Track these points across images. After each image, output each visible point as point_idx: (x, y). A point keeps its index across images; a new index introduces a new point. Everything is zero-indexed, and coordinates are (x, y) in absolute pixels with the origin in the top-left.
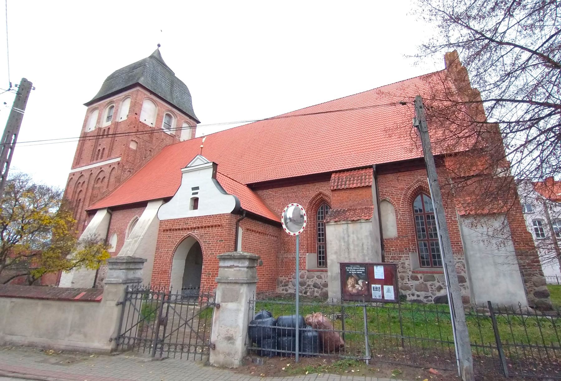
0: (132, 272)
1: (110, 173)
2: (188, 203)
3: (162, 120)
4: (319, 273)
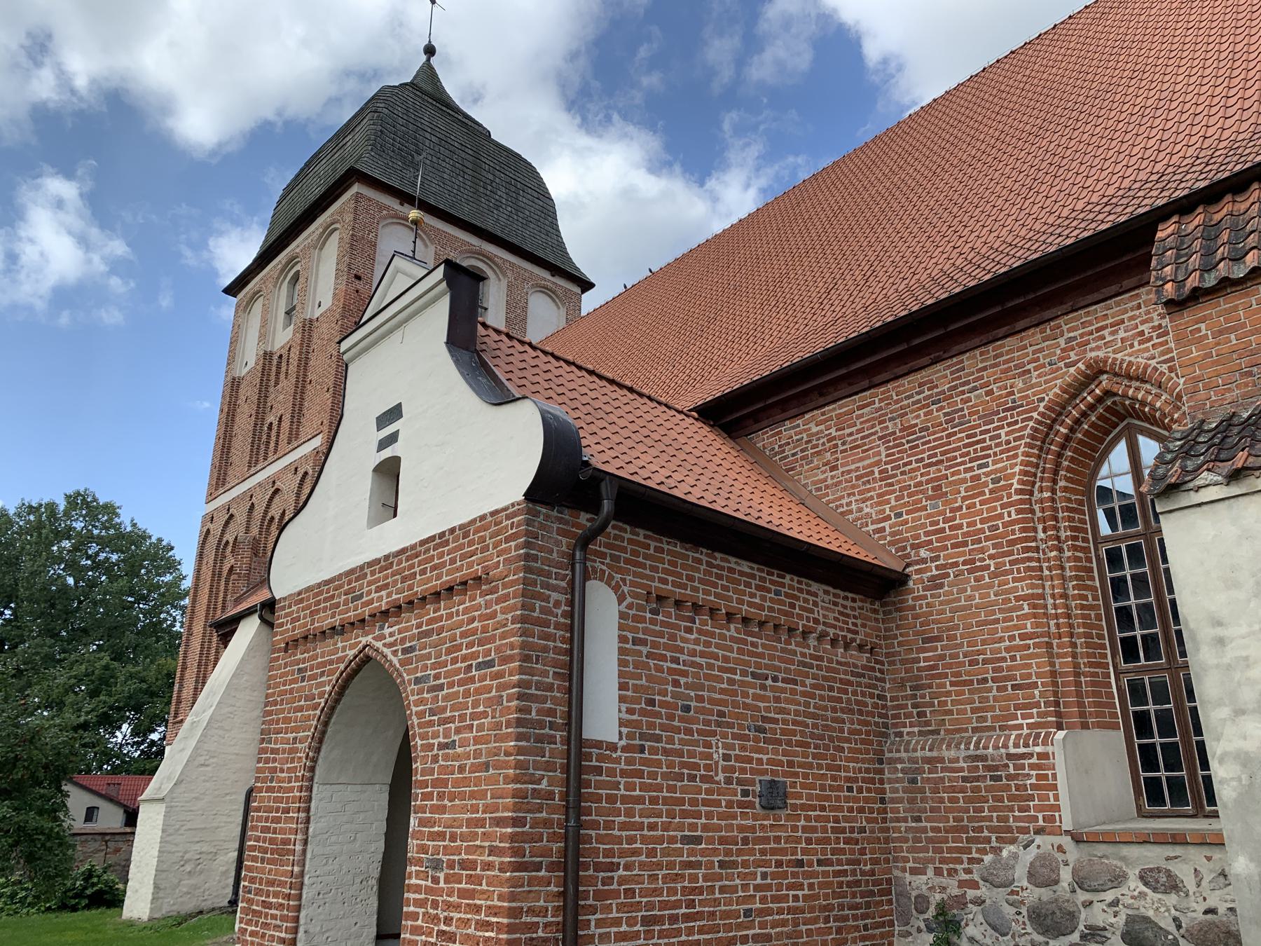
4: (1154, 856)
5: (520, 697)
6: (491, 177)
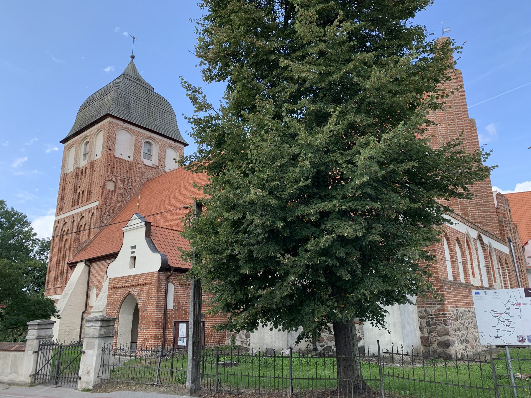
0: (43, 331)
1: (91, 220)
2: (128, 261)
3: (141, 150)
5: (157, 303)
6: (154, 109)
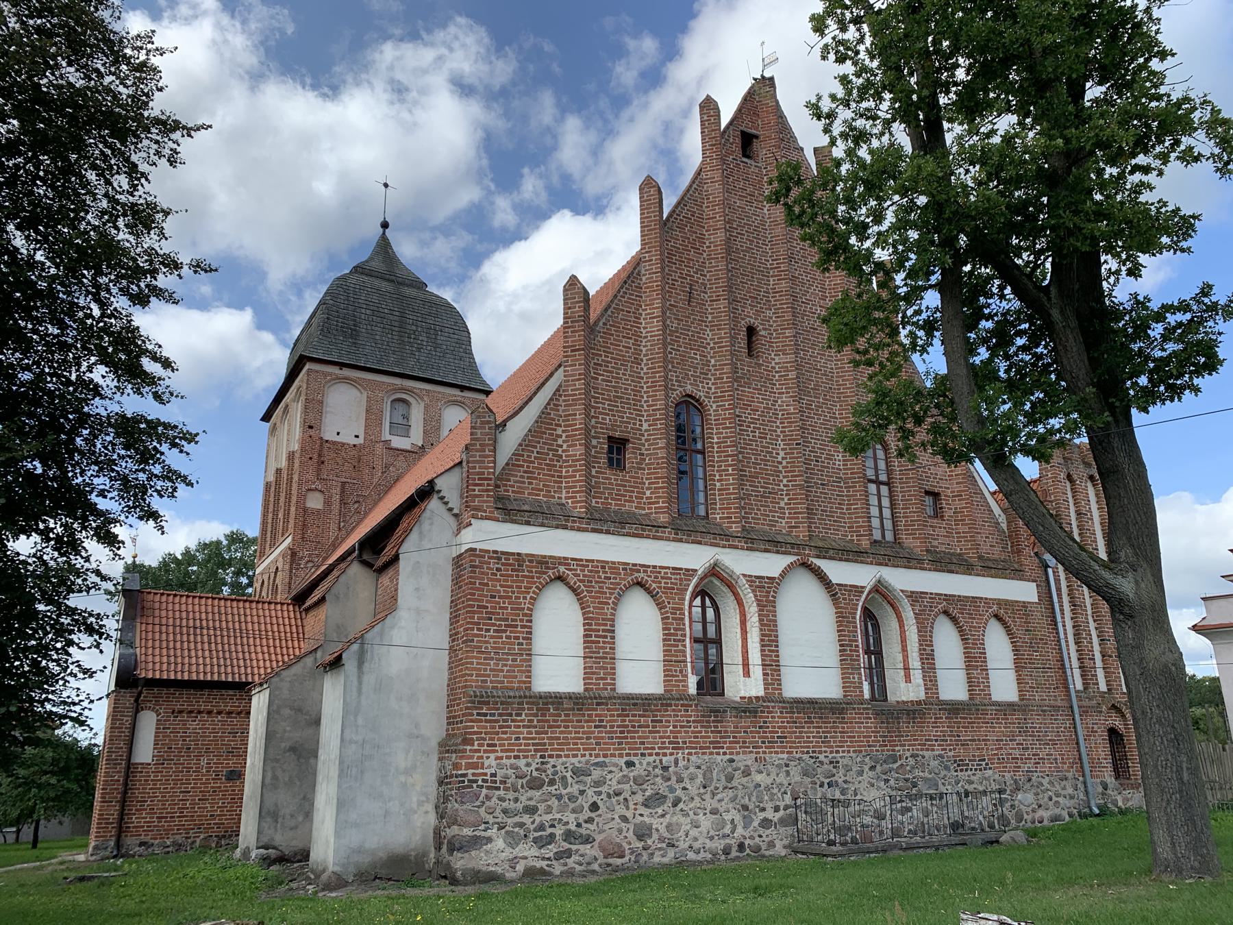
6: (414, 328)
